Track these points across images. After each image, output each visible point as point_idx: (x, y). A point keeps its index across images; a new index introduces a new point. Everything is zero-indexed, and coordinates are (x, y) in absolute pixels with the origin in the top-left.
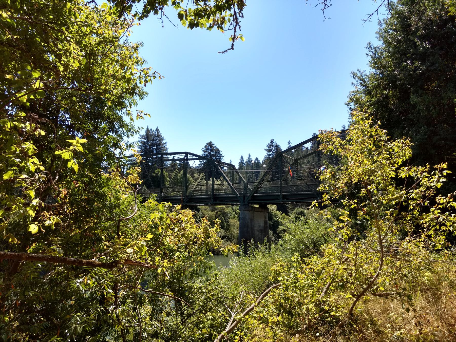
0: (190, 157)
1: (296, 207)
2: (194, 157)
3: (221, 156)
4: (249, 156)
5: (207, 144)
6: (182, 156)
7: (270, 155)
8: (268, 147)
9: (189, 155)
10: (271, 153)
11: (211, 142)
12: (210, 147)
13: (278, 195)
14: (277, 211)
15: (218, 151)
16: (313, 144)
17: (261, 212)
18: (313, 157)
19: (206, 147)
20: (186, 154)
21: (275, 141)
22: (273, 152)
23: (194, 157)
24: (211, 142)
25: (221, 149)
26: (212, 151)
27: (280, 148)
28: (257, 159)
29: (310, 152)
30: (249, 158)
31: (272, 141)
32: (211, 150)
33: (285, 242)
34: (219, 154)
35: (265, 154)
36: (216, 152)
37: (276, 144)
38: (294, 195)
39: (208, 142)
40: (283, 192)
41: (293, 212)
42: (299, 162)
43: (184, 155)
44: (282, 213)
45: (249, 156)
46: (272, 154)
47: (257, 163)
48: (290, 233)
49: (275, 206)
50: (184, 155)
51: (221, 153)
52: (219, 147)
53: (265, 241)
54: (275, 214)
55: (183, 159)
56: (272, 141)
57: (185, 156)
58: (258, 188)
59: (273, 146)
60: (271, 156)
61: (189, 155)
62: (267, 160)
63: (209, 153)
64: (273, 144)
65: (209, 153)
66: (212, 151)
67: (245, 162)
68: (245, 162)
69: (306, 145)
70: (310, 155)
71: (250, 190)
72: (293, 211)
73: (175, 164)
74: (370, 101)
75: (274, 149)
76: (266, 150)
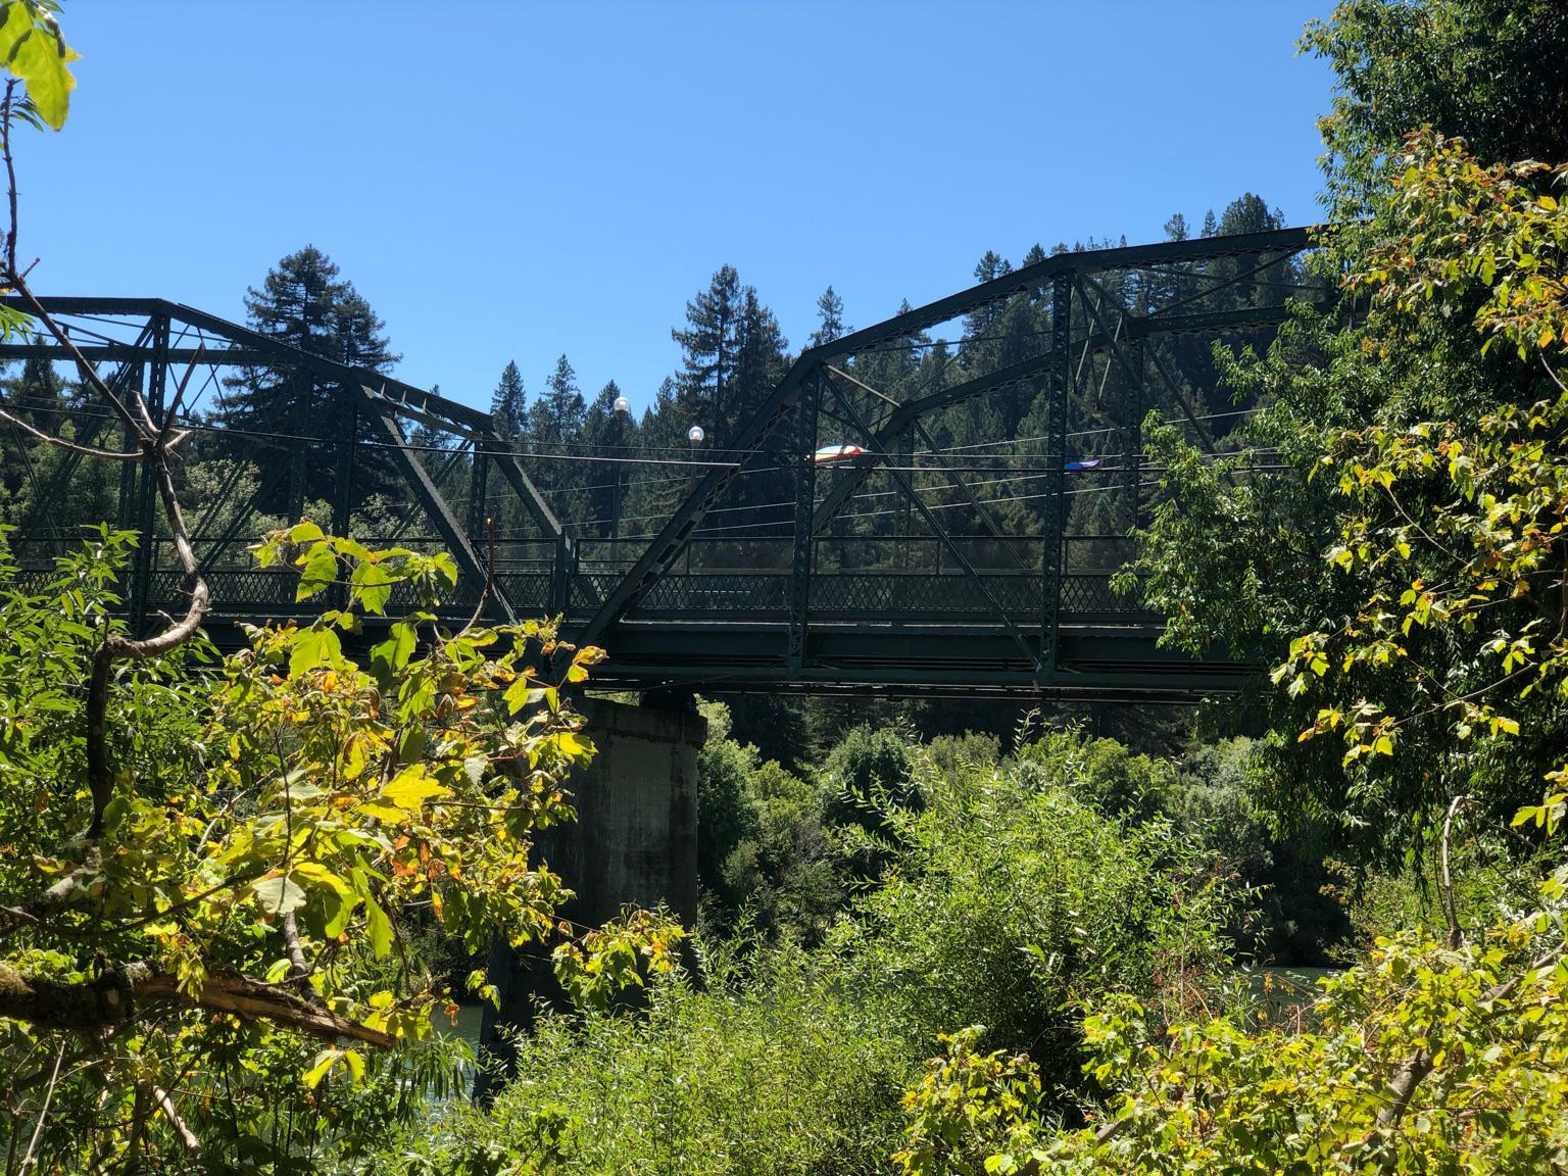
0: (184, 338)
1: (851, 722)
2: (214, 342)
3: (377, 355)
4: (564, 368)
5: (286, 265)
6: (127, 330)
7: (707, 371)
8: (698, 321)
9: (176, 325)
10: (709, 361)
11: (310, 256)
12: (301, 290)
13: (779, 635)
14: (733, 745)
15: (357, 320)
16: (977, 326)
17: (653, 739)
18: (976, 412)
19: (273, 282)
20: (160, 312)
21: (743, 282)
22: (724, 355)
23: (214, 342)
24: (310, 256)
25: (378, 309)
26: (315, 313)
27: (774, 330)
28: (612, 392)
29: (958, 376)
30: (559, 383)
31: (726, 281)
32: (309, 309)
33: (876, 929)
34: (365, 339)
35: (674, 362)
36: (343, 327)
37: (752, 302)
38: (881, 636)
39: (294, 249)
40: (811, 616)
41: (835, 753)
42: (927, 422)
43: (144, 320)
44: (765, 756)
45: (564, 368)
46: (719, 367)
47: (612, 427)
48: (913, 876)
49: (719, 706)
50: (144, 320)
51: (378, 335)
52: (364, 292)
53: (744, 922)
54: (717, 759)
55: (130, 355)
56: (726, 281)
57: (30, 373)
58: (651, 579)
59: (726, 313)
60: (713, 382)
61: (176, 325)
62: (687, 403)
63: (297, 326)
64: (733, 304)
65: (297, 326)
66: (315, 313)
67: (529, 405)
68: (529, 405)
69: (935, 333)
70: (961, 394)
71: (589, 591)
72: (829, 745)
73: (50, 386)
74: (1481, 40)
75: (732, 334)
76: (683, 339)
